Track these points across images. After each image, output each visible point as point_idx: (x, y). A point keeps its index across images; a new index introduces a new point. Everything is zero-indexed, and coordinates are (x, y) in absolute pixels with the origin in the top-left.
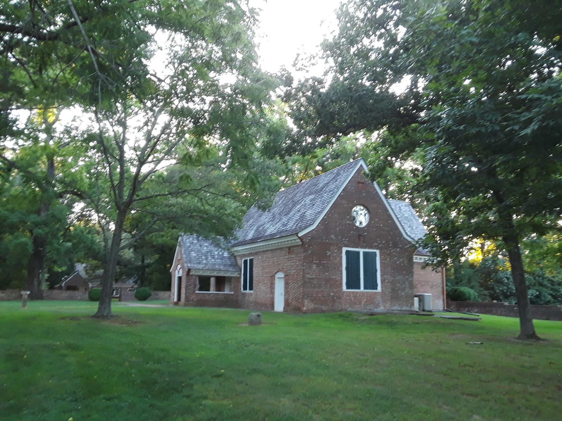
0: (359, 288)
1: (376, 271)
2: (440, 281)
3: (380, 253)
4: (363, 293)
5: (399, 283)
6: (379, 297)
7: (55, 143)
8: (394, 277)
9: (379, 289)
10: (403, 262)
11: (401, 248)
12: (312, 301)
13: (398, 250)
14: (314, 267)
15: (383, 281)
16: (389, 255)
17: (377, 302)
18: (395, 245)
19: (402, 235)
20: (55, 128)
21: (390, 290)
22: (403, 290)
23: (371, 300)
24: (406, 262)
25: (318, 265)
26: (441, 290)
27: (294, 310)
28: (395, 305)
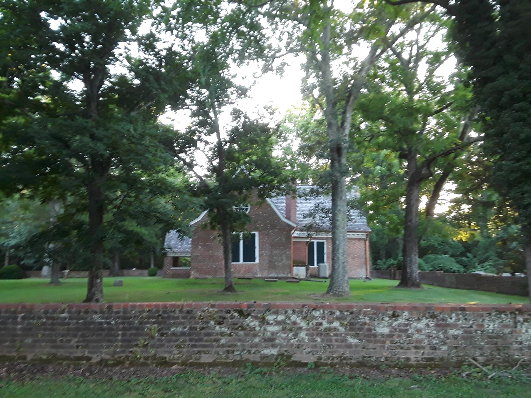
0: (238, 261)
1: (254, 248)
2: (363, 253)
3: (260, 235)
4: (242, 265)
5: (276, 256)
6: (257, 269)
7: (377, 83)
8: (271, 252)
9: (257, 261)
10: (281, 239)
11: (279, 229)
12: (197, 271)
13: (276, 230)
14: (200, 247)
15: (261, 255)
16: (267, 235)
17: (255, 271)
18: (274, 227)
19: (280, 219)
20: (445, 41)
21: (267, 262)
22: (281, 261)
23: (249, 269)
24: (283, 239)
25: (203, 246)
26: (363, 260)
27: (342, 295)
28: (272, 273)
